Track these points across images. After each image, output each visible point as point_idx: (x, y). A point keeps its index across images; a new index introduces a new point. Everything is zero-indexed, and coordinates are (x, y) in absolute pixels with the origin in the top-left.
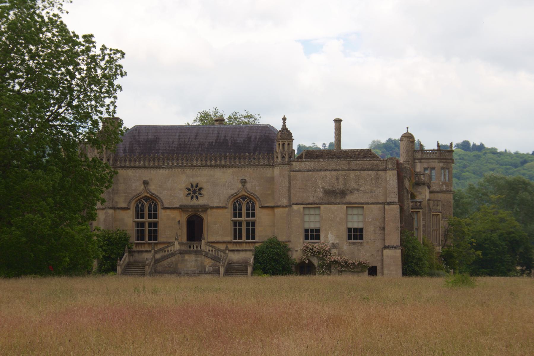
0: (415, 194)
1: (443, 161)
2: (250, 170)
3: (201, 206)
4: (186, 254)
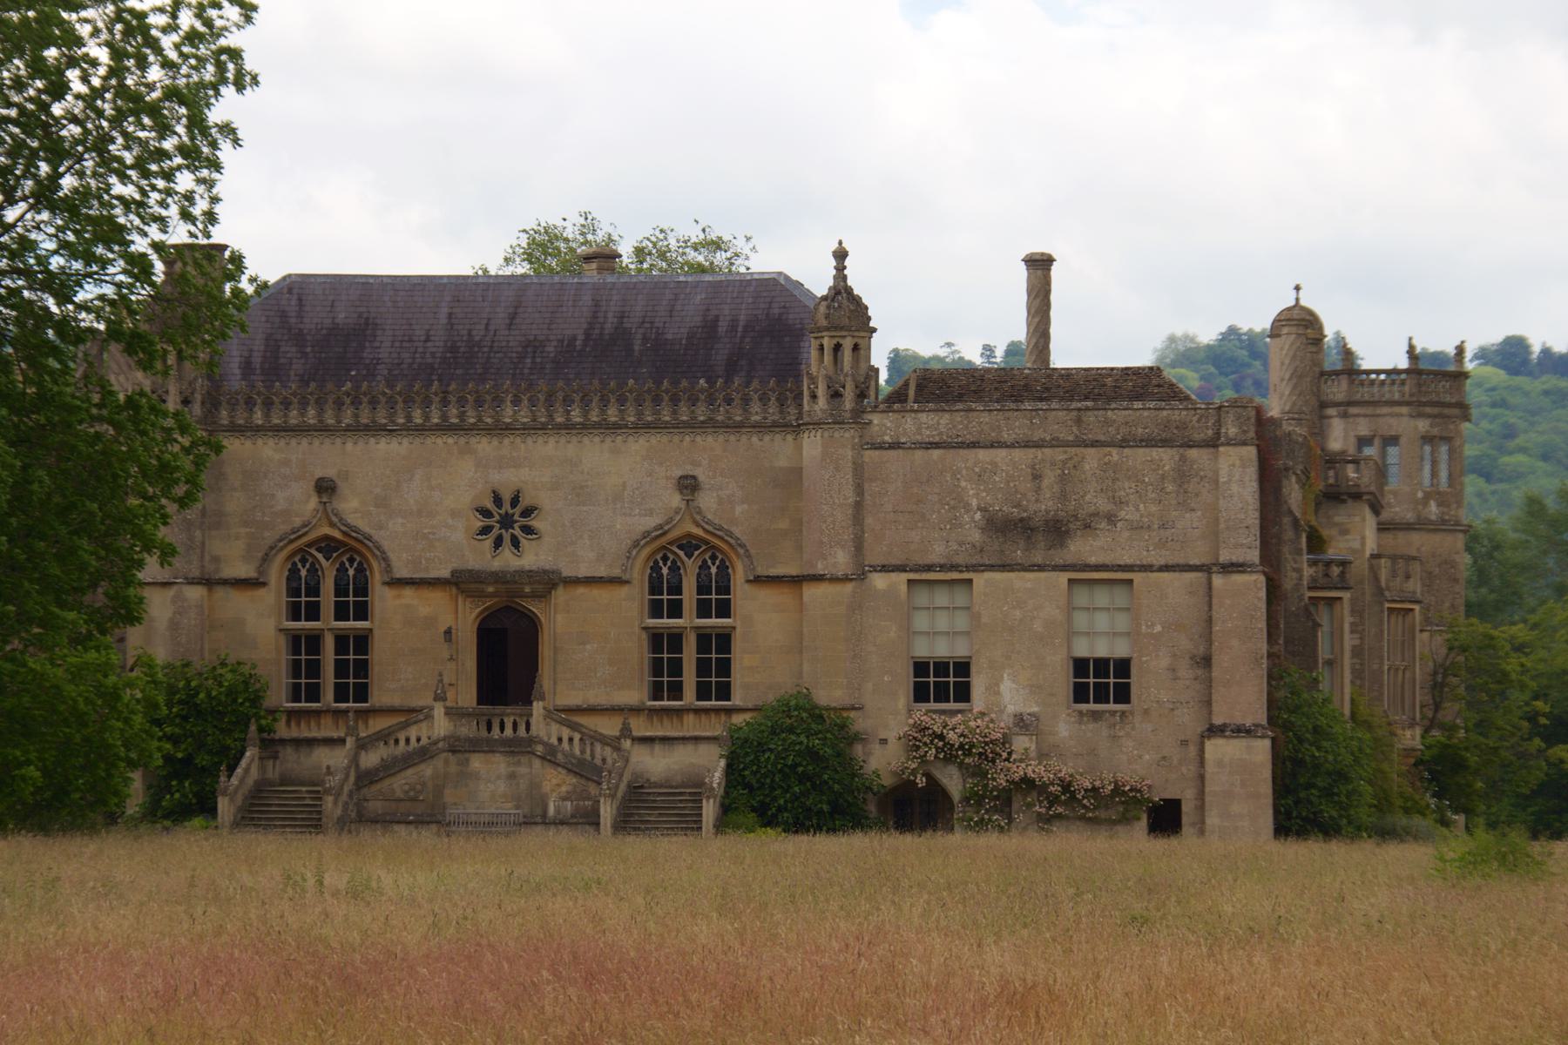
0: (1325, 533)
1: (1428, 410)
2: (711, 443)
3: (530, 574)
4: (474, 751)
